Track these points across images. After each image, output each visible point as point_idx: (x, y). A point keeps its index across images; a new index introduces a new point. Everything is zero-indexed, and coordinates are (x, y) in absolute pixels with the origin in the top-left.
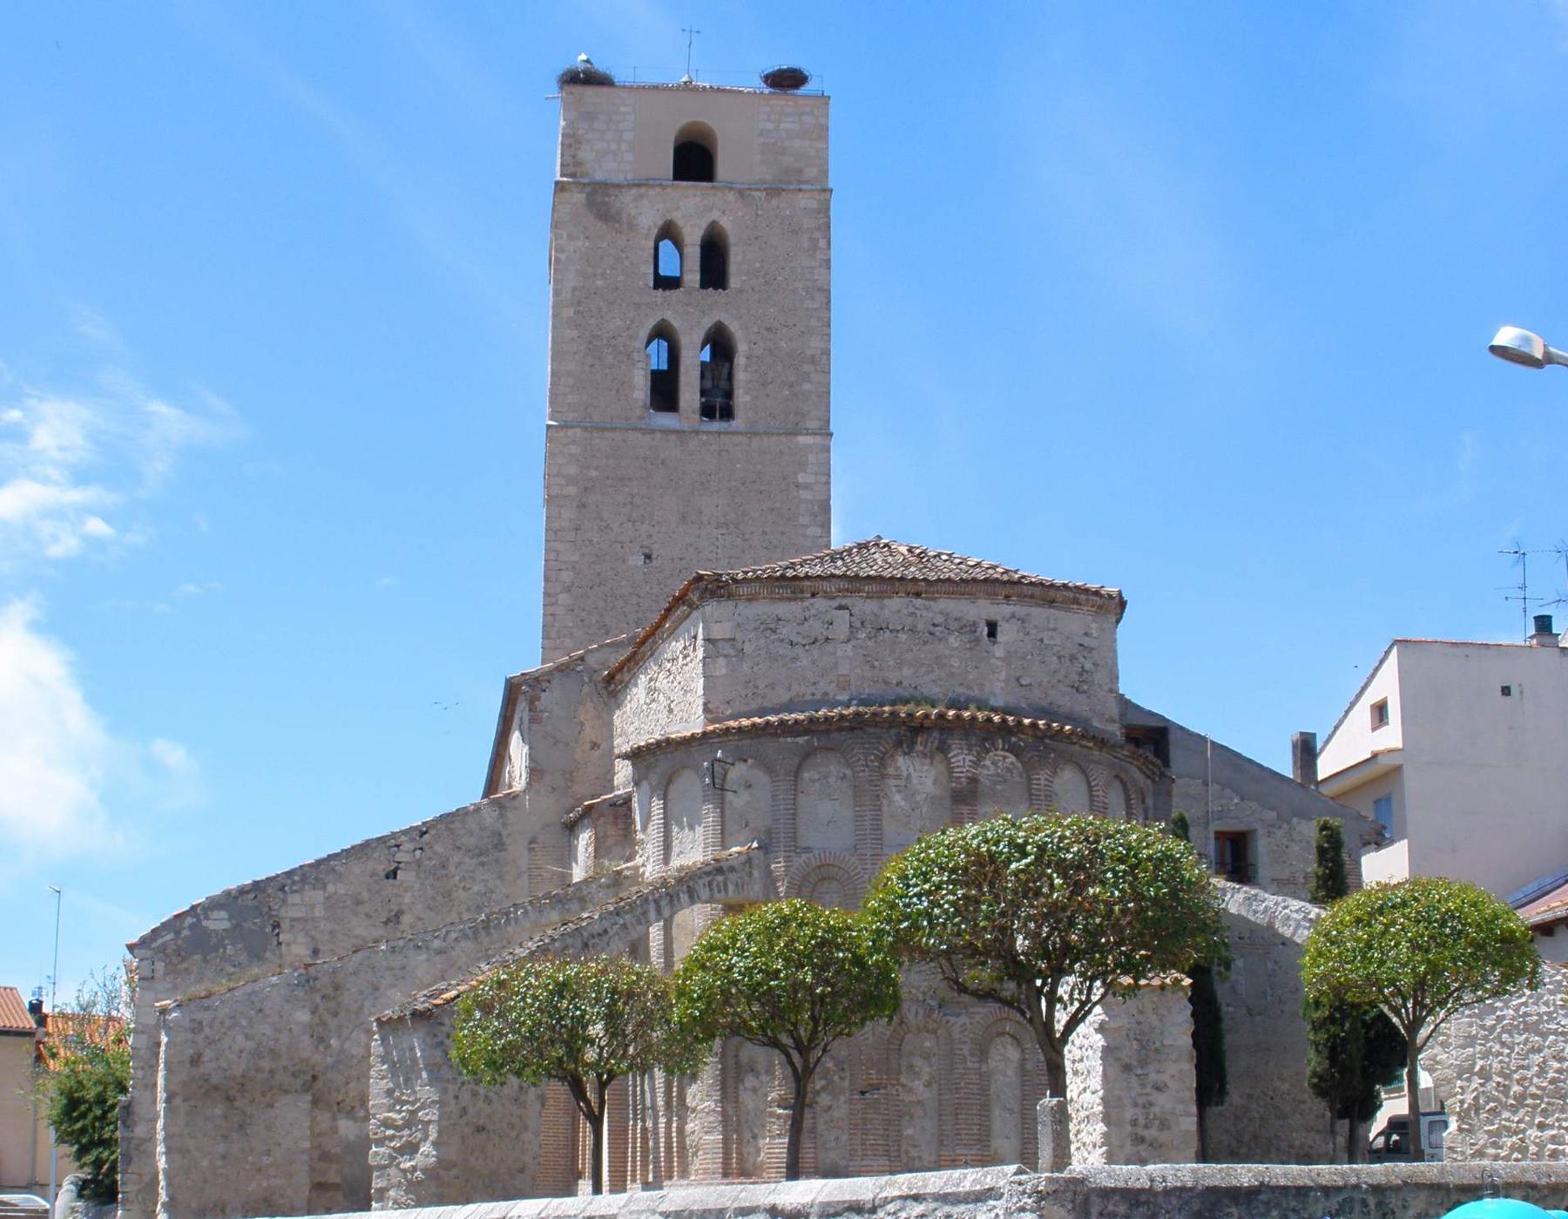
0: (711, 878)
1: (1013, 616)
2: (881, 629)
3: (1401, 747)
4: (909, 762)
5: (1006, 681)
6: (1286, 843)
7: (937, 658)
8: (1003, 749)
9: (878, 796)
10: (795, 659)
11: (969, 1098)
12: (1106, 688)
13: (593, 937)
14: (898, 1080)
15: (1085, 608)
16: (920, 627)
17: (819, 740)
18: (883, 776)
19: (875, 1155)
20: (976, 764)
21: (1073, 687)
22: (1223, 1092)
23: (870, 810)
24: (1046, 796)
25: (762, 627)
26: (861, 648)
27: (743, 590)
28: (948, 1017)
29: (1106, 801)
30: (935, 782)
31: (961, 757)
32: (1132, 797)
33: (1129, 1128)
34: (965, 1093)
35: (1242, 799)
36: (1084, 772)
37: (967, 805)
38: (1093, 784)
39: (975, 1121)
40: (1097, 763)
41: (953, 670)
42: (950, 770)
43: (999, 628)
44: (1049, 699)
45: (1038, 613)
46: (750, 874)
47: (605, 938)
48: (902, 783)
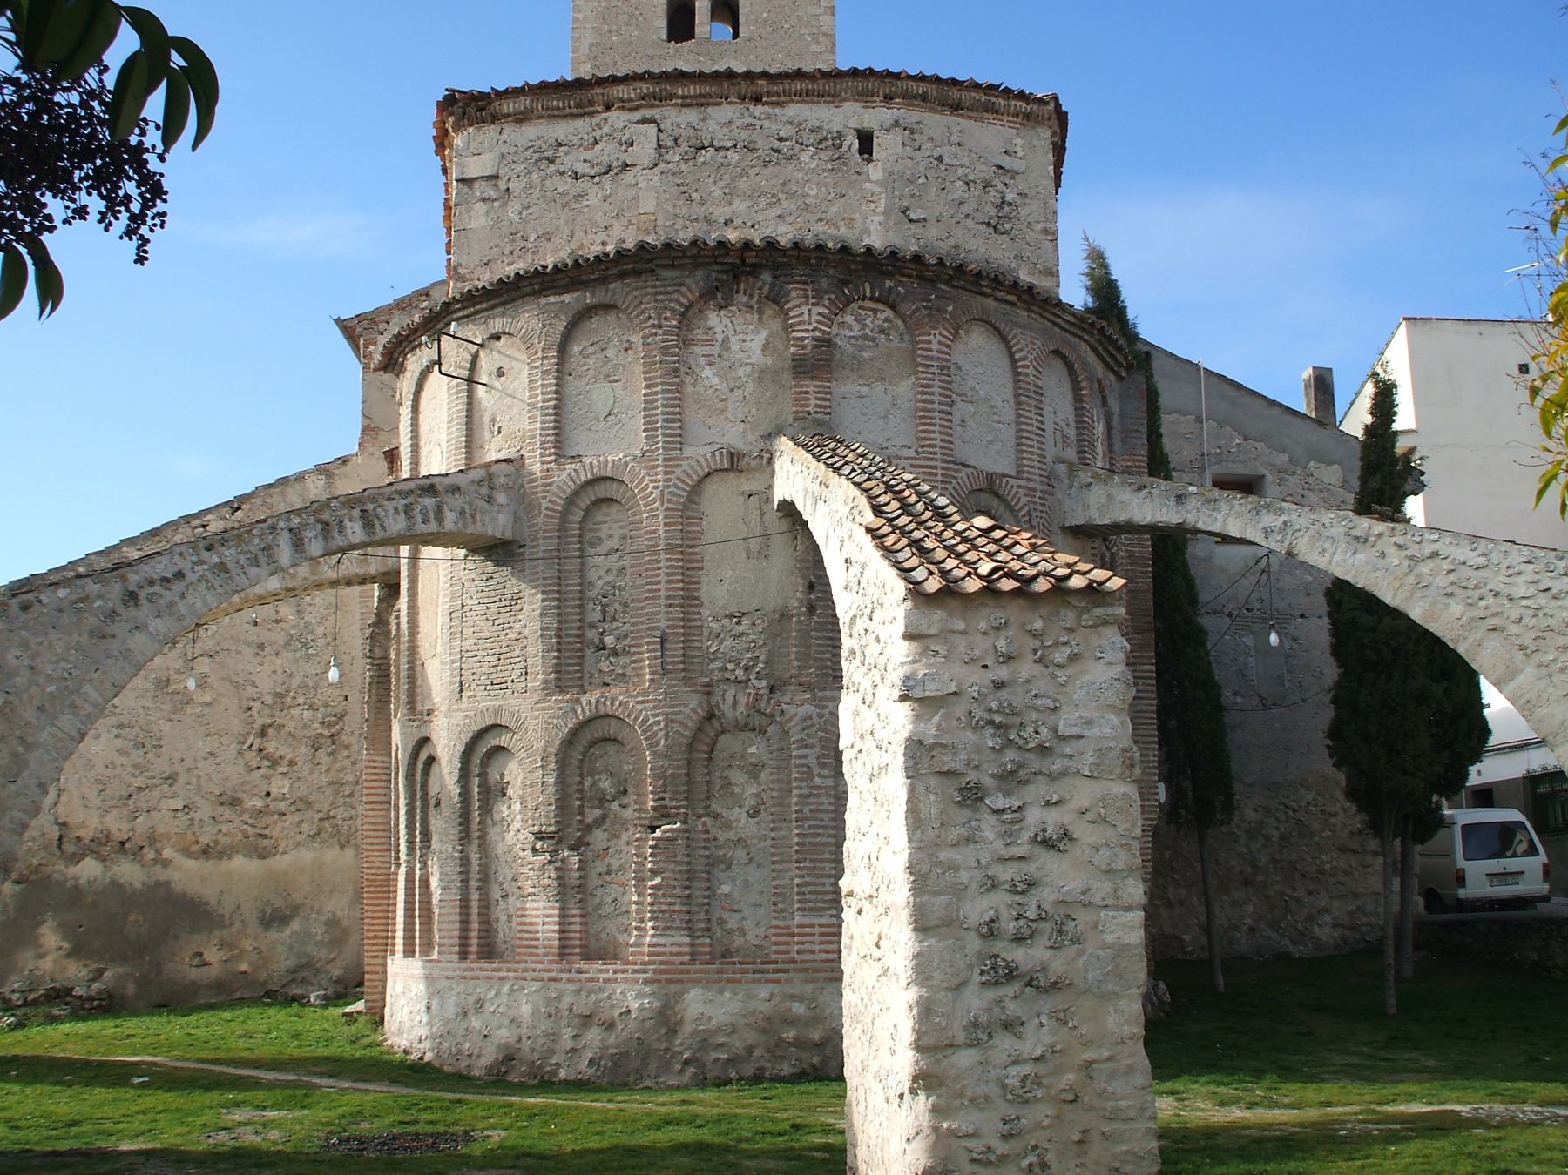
0: (410, 499)
1: (896, 123)
2: (704, 148)
3: (1413, 427)
4: (727, 321)
5: (886, 213)
6: (1302, 492)
7: (784, 184)
8: (871, 299)
9: (676, 370)
10: (581, 196)
11: (819, 835)
12: (1039, 227)
13: (151, 583)
14: (708, 807)
15: (1006, 118)
16: (760, 143)
17: (593, 294)
18: (688, 342)
19: (668, 928)
20: (828, 319)
21: (988, 224)
22: (1229, 805)
23: (663, 392)
24: (942, 368)
25: (536, 156)
26: (673, 174)
27: (509, 106)
28: (784, 706)
29: (1039, 383)
30: (765, 347)
31: (805, 309)
32: (1084, 384)
33: (974, 943)
34: (810, 827)
35: (1246, 439)
36: (1004, 339)
37: (812, 379)
38: (1017, 356)
39: (827, 871)
40: (1024, 327)
41: (808, 201)
42: (788, 329)
43: (875, 140)
44: (952, 241)
45: (936, 123)
46: (489, 499)
47: (178, 587)
48: (716, 350)
